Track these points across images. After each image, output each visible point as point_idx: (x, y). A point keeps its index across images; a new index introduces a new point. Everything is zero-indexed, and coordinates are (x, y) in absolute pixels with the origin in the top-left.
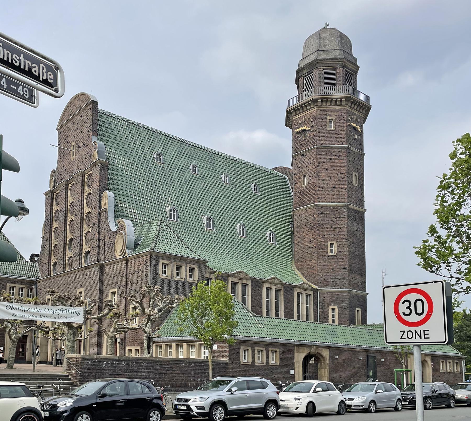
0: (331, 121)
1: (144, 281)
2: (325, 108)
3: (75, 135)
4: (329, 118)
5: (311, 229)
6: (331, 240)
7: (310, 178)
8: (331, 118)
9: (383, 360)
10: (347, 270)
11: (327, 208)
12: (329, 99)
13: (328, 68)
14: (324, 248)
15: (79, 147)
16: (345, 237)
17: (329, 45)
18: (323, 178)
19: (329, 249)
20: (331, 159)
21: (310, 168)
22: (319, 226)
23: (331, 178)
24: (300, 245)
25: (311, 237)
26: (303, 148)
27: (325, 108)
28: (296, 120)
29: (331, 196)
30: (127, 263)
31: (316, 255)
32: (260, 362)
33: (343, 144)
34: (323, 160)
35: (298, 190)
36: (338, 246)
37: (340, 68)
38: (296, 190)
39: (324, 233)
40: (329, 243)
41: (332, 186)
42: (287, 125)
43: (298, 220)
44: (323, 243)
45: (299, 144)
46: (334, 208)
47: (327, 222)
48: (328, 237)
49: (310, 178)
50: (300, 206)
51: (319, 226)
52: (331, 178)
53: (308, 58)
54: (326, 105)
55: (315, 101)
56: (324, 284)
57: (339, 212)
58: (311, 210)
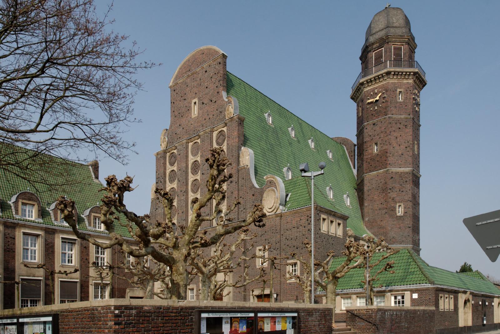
0: (400, 92)
1: (307, 236)
2: (396, 81)
3: (197, 92)
4: (399, 90)
5: (383, 193)
6: (399, 202)
7: (381, 146)
8: (400, 90)
9: (487, 303)
10: (411, 228)
11: (397, 173)
12: (380, 75)
13: (396, 43)
14: (394, 210)
15: (203, 103)
16: (410, 199)
17: (396, 22)
18: (393, 145)
19: (397, 210)
20: (400, 128)
21: (382, 136)
22: (390, 189)
23: (400, 145)
24: (371, 207)
25: (382, 200)
26: (375, 117)
27: (396, 81)
28: (367, 91)
29: (400, 162)
30: (281, 219)
31: (387, 215)
32: (447, 307)
33: (409, 115)
34: (393, 129)
35: (369, 156)
36: (405, 208)
37: (406, 44)
38: (367, 157)
39: (393, 196)
40: (398, 204)
41: (400, 153)
42: (354, 98)
43: (368, 184)
44: (393, 205)
45: (370, 114)
46: (401, 173)
47: (396, 186)
48: (397, 199)
49: (381, 146)
50: (370, 171)
51: (390, 189)
52: (400, 145)
53: (379, 33)
54: (383, 80)
55: (388, 73)
56: (393, 241)
57: (406, 177)
58: (382, 175)
